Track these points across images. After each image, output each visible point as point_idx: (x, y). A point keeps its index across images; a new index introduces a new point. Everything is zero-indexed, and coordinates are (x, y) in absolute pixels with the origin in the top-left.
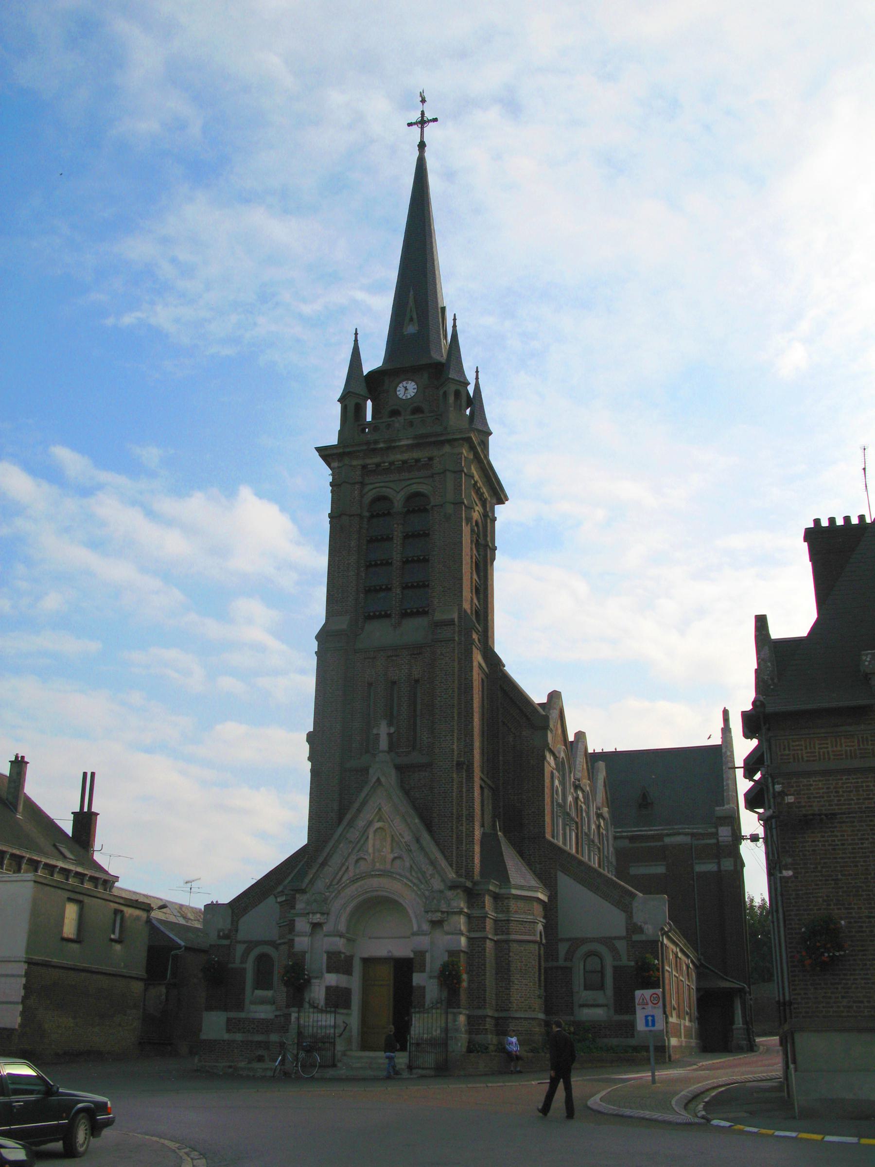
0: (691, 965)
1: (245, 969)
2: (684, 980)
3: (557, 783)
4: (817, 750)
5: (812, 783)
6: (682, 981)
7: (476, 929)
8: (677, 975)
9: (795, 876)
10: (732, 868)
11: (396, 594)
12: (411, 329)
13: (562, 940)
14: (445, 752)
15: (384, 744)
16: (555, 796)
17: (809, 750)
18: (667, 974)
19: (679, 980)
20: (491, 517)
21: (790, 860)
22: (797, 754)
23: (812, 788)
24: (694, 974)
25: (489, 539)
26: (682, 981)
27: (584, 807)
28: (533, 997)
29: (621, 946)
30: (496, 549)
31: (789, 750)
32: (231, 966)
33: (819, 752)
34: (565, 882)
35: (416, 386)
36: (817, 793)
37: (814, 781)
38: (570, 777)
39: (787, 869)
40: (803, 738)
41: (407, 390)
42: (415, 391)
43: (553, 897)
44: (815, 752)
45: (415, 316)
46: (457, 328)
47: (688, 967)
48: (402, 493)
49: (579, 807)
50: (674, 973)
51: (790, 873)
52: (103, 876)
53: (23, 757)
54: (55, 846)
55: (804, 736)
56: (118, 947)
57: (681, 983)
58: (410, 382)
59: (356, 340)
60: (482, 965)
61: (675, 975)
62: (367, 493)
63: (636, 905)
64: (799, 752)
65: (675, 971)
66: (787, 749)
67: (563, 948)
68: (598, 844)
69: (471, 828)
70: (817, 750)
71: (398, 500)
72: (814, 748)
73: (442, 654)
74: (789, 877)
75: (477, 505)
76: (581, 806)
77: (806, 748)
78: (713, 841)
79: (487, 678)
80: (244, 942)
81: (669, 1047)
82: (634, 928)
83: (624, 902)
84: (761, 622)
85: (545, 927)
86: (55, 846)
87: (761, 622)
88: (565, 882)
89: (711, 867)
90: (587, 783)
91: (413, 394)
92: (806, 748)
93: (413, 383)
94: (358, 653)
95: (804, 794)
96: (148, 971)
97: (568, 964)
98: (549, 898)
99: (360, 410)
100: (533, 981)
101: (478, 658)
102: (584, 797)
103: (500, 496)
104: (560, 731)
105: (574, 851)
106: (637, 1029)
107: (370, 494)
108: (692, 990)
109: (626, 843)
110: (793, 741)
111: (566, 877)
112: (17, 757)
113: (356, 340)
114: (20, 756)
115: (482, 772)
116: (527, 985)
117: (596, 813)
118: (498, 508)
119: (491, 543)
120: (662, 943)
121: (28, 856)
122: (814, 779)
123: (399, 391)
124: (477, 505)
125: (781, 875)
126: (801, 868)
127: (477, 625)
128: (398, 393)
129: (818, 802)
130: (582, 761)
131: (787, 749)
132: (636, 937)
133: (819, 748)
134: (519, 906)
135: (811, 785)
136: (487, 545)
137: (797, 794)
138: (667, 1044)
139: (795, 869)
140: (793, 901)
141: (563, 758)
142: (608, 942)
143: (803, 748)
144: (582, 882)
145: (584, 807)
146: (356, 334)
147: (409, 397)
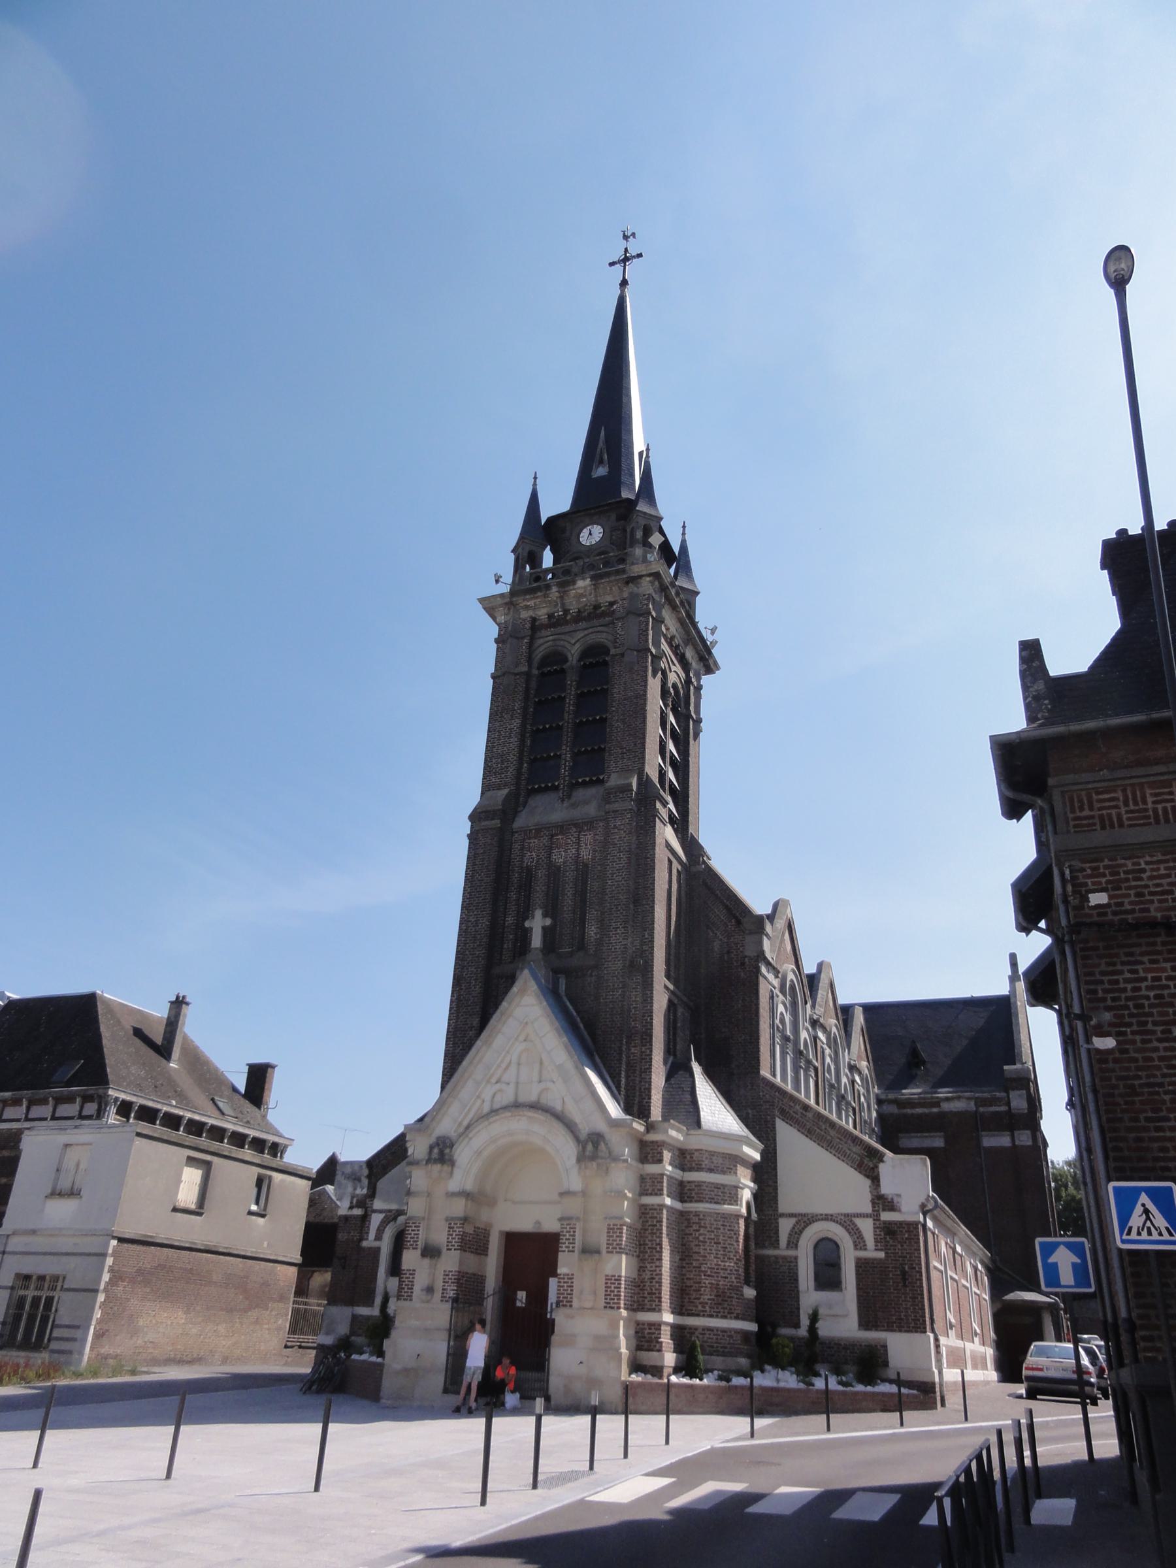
0: (980, 1267)
1: (378, 1249)
2: (968, 1285)
3: (862, 1099)
4: (1150, 805)
5: (1143, 866)
6: (964, 1286)
7: (650, 1192)
8: (978, 1292)
9: (1121, 1048)
10: (1030, 1143)
11: (566, 762)
12: (601, 471)
13: (782, 1215)
14: (615, 949)
15: (536, 941)
16: (827, 1075)
17: (1132, 807)
18: (934, 1274)
19: (981, 1299)
20: (695, 683)
21: (1107, 1016)
22: (1110, 815)
23: (1144, 876)
24: (986, 1278)
25: (692, 708)
26: (967, 1288)
27: (862, 1091)
28: (735, 1296)
29: (867, 1227)
30: (701, 722)
31: (1091, 809)
32: (365, 1244)
33: (1155, 811)
34: (785, 1133)
35: (602, 530)
36: (1158, 885)
37: (1147, 863)
38: (844, 1056)
39: (1103, 1034)
40: (1118, 786)
41: (592, 535)
42: (601, 535)
43: (770, 1155)
44: (1146, 810)
45: (606, 457)
46: (650, 459)
47: (976, 1269)
48: (578, 645)
49: (819, 1048)
50: (950, 1273)
51: (1108, 1043)
52: (272, 1138)
53: (184, 997)
54: (213, 1100)
55: (1119, 782)
56: (261, 1221)
57: (962, 1291)
58: (595, 526)
59: (535, 484)
60: (657, 1245)
61: (952, 1278)
62: (539, 646)
63: (884, 1170)
64: (1114, 812)
65: (951, 1270)
66: (1086, 807)
67: (785, 1227)
68: (853, 1103)
69: (648, 1051)
70: (1150, 805)
71: (574, 652)
72: (1145, 802)
73: (615, 827)
74: (1109, 1052)
75: (674, 664)
76: (859, 1091)
77: (1126, 804)
78: (1003, 1108)
79: (686, 870)
80: (380, 1211)
81: (941, 1385)
82: (882, 1202)
83: (868, 1164)
84: (1031, 652)
85: (756, 1196)
86: (213, 1100)
87: (1031, 652)
88: (785, 1133)
89: (1004, 1141)
90: (790, 969)
91: (598, 539)
92: (1126, 804)
93: (599, 527)
94: (516, 832)
95: (1129, 888)
96: (303, 1253)
97: (791, 1253)
98: (763, 1154)
99: (534, 559)
100: (735, 1273)
101: (667, 834)
102: (862, 1080)
103: (708, 664)
104: (789, 947)
105: (812, 1102)
106: (490, 1337)
107: (542, 648)
108: (984, 1302)
109: (893, 1109)
110: (1098, 793)
111: (784, 1124)
112: (178, 997)
113: (535, 484)
114: (181, 995)
115: (668, 976)
116: (726, 1278)
117: (810, 1019)
118: (706, 680)
119: (695, 713)
120: (924, 1226)
121: (165, 1109)
122: (1148, 859)
123: (583, 537)
124: (674, 664)
125: (1090, 1046)
126: (1133, 1033)
127: (661, 792)
128: (581, 540)
129: (1160, 901)
130: (825, 994)
131: (1086, 807)
132: (886, 1216)
133: (1154, 802)
134: (715, 1162)
135: (1144, 871)
136: (689, 716)
137: (1114, 889)
138: (937, 1379)
139: (1119, 1034)
140: (1120, 1100)
141: (835, 1034)
142: (847, 1221)
143: (1121, 804)
144: (809, 1133)
145: (862, 1091)
146: (535, 478)
147: (594, 543)
